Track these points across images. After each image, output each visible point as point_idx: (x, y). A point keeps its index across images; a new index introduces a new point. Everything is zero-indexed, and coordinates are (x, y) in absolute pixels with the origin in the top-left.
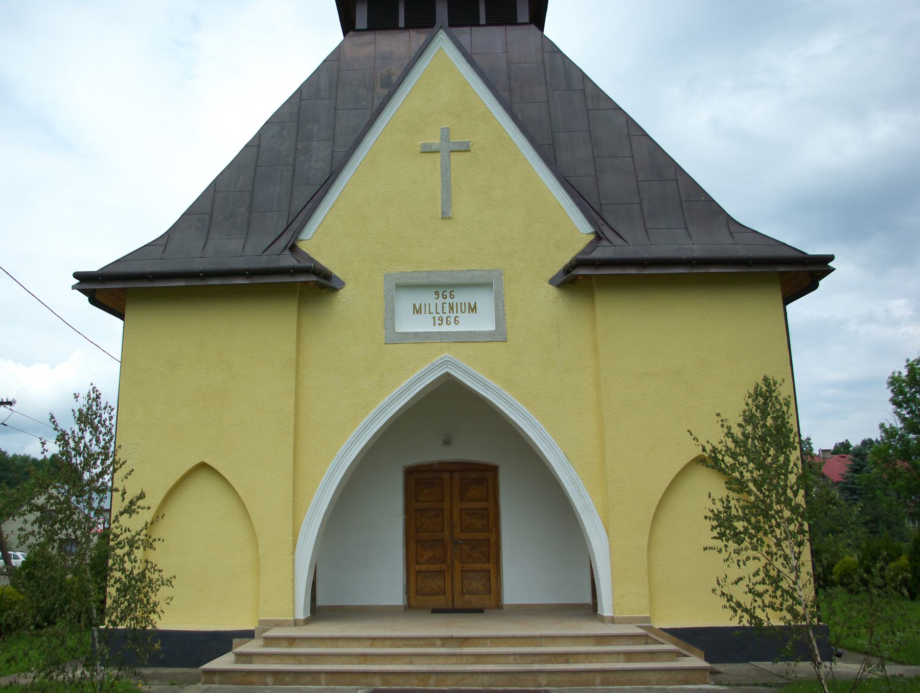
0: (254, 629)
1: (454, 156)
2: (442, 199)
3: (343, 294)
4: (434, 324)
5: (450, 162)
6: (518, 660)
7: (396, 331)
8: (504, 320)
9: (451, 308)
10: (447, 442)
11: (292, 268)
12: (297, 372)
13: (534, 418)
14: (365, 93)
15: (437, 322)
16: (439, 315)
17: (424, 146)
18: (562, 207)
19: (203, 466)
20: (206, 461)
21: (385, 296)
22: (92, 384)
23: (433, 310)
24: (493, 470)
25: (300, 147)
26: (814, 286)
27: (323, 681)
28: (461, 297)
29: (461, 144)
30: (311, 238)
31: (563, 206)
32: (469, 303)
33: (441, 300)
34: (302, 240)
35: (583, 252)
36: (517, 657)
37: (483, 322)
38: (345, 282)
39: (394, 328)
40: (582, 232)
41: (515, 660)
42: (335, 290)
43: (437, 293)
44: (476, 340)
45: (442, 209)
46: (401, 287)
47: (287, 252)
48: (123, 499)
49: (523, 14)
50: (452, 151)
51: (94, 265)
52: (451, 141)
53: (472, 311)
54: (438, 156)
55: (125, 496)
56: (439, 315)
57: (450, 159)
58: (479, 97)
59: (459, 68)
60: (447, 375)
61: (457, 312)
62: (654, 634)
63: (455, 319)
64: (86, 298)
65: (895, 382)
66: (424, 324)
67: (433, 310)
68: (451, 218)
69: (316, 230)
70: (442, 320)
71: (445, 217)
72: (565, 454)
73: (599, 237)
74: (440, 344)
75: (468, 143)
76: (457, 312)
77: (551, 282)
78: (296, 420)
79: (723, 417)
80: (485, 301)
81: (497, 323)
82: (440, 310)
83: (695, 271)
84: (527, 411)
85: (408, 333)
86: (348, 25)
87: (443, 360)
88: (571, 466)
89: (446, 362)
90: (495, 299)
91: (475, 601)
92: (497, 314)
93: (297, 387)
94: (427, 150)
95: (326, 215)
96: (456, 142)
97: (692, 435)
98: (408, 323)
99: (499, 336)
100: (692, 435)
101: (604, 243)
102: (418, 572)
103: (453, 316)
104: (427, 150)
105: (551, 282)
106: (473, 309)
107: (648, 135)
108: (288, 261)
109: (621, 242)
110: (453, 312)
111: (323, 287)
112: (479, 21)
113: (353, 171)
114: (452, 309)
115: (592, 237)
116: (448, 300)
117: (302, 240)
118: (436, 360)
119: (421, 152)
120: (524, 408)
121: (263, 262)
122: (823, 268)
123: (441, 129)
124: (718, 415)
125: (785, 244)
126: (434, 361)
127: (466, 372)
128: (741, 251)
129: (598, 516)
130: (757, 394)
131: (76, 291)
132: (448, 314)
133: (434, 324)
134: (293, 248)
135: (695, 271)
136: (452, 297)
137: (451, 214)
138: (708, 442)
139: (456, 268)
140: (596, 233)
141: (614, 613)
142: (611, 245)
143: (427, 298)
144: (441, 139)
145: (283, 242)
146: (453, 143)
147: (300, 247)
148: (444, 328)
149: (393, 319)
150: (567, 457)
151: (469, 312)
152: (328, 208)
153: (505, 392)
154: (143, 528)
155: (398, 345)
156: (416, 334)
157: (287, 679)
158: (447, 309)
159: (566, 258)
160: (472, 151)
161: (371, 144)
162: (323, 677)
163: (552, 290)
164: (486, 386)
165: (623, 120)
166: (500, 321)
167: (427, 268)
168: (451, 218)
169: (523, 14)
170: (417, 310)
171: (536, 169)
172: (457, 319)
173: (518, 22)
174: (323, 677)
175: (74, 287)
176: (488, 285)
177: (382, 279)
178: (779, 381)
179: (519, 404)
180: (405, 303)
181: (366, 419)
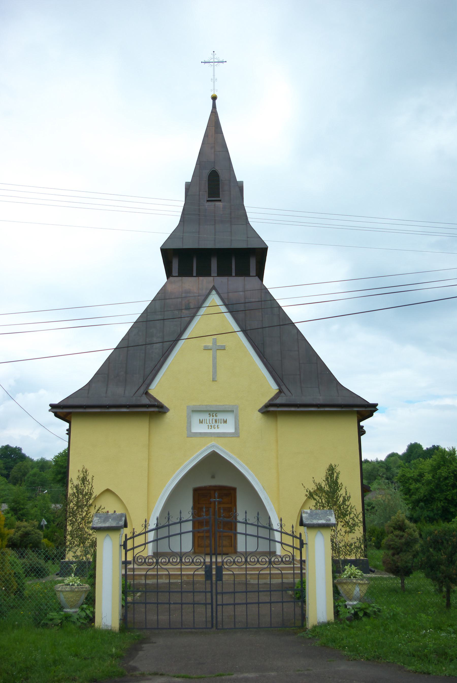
0: (131, 560)
1: (218, 351)
2: (213, 372)
3: (168, 414)
4: (208, 428)
5: (216, 355)
6: (239, 570)
7: (192, 432)
8: (239, 427)
9: (216, 421)
10: (213, 477)
11: (148, 405)
12: (149, 449)
13: (250, 471)
14: (177, 313)
15: (209, 427)
16: (210, 424)
17: (205, 346)
18: (265, 377)
19: (108, 491)
20: (109, 488)
21: (187, 416)
22: (83, 466)
23: (208, 422)
24: (234, 489)
25: (148, 341)
26: (371, 415)
27: (164, 578)
28: (221, 416)
29: (222, 346)
30: (155, 388)
31: (266, 377)
32: (224, 419)
33: (211, 417)
34: (150, 389)
35: (272, 399)
36: (239, 569)
37: (229, 428)
38: (170, 409)
39: (191, 430)
40: (273, 388)
41: (238, 570)
42: (165, 413)
43: (210, 414)
44: (226, 436)
45: (212, 377)
46: (194, 411)
47: (144, 396)
48: (95, 509)
49: (253, 271)
50: (217, 349)
51: (56, 401)
52: (217, 345)
53: (225, 423)
54: (211, 351)
55: (96, 507)
56: (210, 424)
57: (216, 353)
58: (230, 323)
59: (221, 309)
60: (214, 451)
61: (218, 423)
62: (297, 562)
63: (217, 426)
64: (53, 414)
65: (433, 445)
66: (203, 429)
67: (208, 422)
68: (217, 381)
69: (157, 385)
70: (212, 427)
71: (214, 380)
72: (263, 487)
73: (281, 391)
74: (211, 438)
75: (224, 346)
76: (218, 423)
77: (260, 411)
78: (148, 470)
79: (314, 479)
80: (230, 418)
81: (236, 429)
82: (211, 422)
83: (319, 409)
84: (247, 468)
85: (197, 433)
86: (169, 273)
87: (212, 445)
88: (265, 492)
89: (213, 446)
90: (235, 418)
91: (225, 550)
92: (235, 425)
93: (149, 456)
94: (206, 348)
95: (161, 378)
96: (219, 345)
97: (303, 485)
98: (197, 428)
99: (236, 434)
100: (303, 485)
101: (282, 394)
102: (199, 537)
103: (216, 425)
104: (206, 348)
105: (260, 411)
106: (225, 422)
107: (306, 340)
108: (145, 401)
109: (290, 394)
110: (217, 423)
111: (159, 412)
112: (232, 275)
113: (173, 358)
114: (216, 422)
115: (278, 391)
116: (215, 418)
117: (150, 389)
118: (209, 445)
119: (204, 349)
120: (246, 466)
121: (133, 401)
122: (374, 409)
123: (213, 339)
124: (313, 478)
125: (360, 397)
126: (208, 445)
127: (222, 450)
128: (340, 401)
129: (276, 513)
130: (329, 470)
131: (51, 412)
132: (214, 424)
133: (208, 428)
134: (147, 393)
135: (319, 409)
136: (216, 416)
137: (216, 379)
138: (308, 489)
139: (218, 404)
140: (279, 389)
141: (281, 554)
142: (285, 395)
143: (206, 417)
144: (213, 343)
145: (142, 390)
146: (218, 346)
147: (149, 392)
148: (213, 431)
149: (190, 426)
150: (263, 488)
151: (224, 423)
152: (162, 375)
153: (238, 459)
154: (332, 544)
155: (192, 438)
156: (201, 433)
157: (150, 577)
158: (214, 422)
159: (265, 400)
160: (226, 350)
161: (181, 345)
162: (164, 576)
163: (260, 414)
164: (188, 464)
165: (296, 331)
166: (236, 428)
167: (206, 403)
168: (217, 381)
169: (253, 271)
170: (201, 422)
171: (254, 358)
172: (218, 426)
173: (251, 275)
174: (164, 576)
175: (50, 411)
176: (232, 411)
177: (186, 408)
178: (337, 465)
179: (244, 465)
180: (196, 418)
181: (178, 471)
